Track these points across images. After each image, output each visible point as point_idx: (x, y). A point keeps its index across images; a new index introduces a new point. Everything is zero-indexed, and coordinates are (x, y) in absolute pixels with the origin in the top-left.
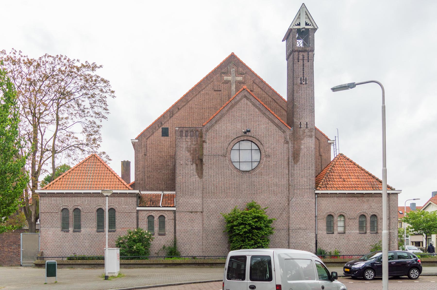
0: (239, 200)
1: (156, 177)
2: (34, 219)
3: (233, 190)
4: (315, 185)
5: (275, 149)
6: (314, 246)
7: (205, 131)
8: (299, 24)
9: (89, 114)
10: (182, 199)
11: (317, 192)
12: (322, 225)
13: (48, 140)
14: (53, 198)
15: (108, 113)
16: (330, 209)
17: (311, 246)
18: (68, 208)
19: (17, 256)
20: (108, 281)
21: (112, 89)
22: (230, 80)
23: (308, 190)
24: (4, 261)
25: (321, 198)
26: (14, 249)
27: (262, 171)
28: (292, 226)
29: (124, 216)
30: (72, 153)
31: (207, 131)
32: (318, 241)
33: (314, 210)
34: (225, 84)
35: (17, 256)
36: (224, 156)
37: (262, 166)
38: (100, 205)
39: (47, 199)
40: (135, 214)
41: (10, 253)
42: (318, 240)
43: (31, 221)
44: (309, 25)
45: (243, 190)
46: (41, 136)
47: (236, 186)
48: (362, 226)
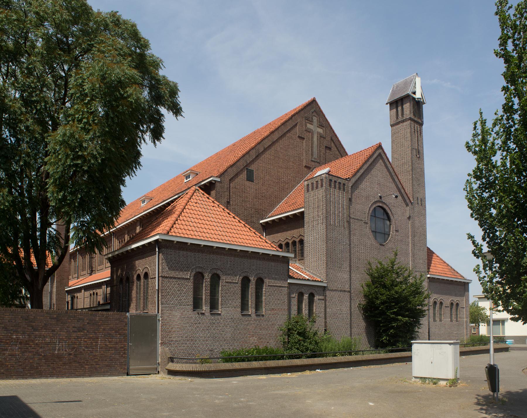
14: (181, 252)
20: (522, 388)
24: (98, 366)
26: (116, 343)
35: (122, 356)
41: (109, 350)
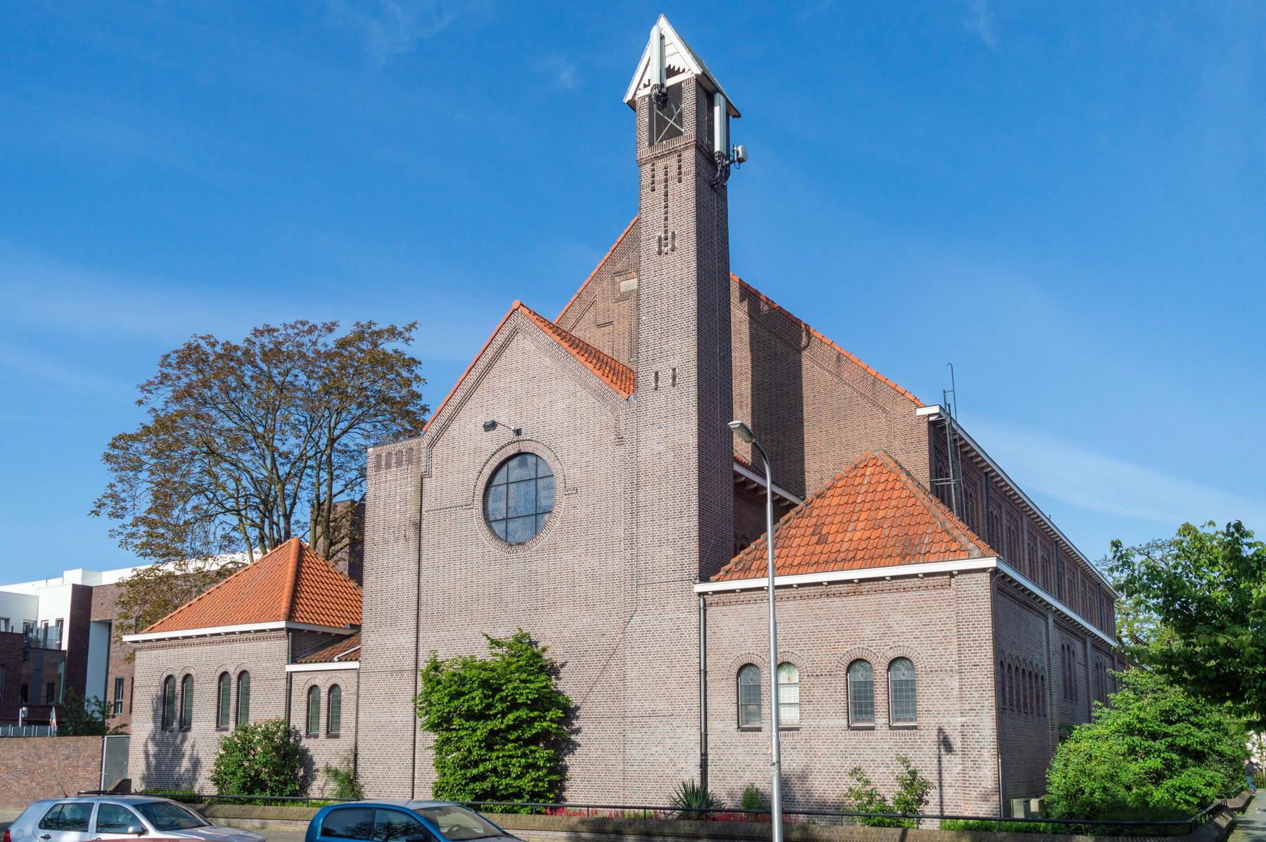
6: (695, 774)
12: (723, 700)
16: (749, 644)
23: (678, 584)
25: (720, 608)
37: (558, 523)
40: (284, 682)
45: (509, 600)
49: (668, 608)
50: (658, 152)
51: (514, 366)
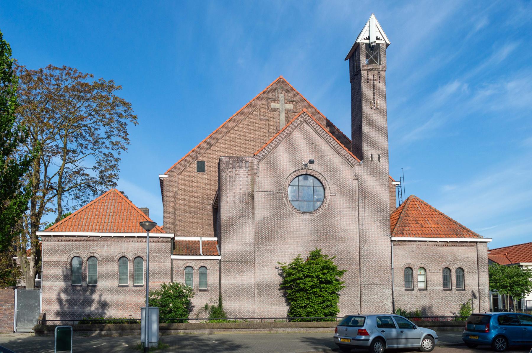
0: (300, 248)
1: (190, 221)
2: (33, 272)
3: (292, 235)
4: (390, 230)
5: (342, 186)
6: (391, 306)
7: (257, 162)
8: (367, 37)
9: (104, 145)
10: (228, 245)
11: (393, 239)
12: (400, 280)
13: (50, 177)
14: (60, 243)
15: (128, 143)
17: (387, 305)
18: (81, 255)
19: (10, 319)
21: (134, 114)
22: (278, 107)
23: (382, 237)
25: (398, 246)
26: (5, 310)
27: (327, 213)
28: (364, 281)
29: (155, 267)
30: (81, 194)
31: (259, 162)
32: (395, 299)
33: (389, 262)
34: (272, 112)
36: (280, 192)
37: (327, 206)
38: (123, 252)
39: (53, 243)
40: (169, 264)
42: (395, 297)
43: (29, 275)
44: (380, 39)
45: (304, 235)
46: (44, 167)
47: (295, 231)
48: (446, 283)
49: (378, 245)
50: (371, 68)
51: (302, 136)
